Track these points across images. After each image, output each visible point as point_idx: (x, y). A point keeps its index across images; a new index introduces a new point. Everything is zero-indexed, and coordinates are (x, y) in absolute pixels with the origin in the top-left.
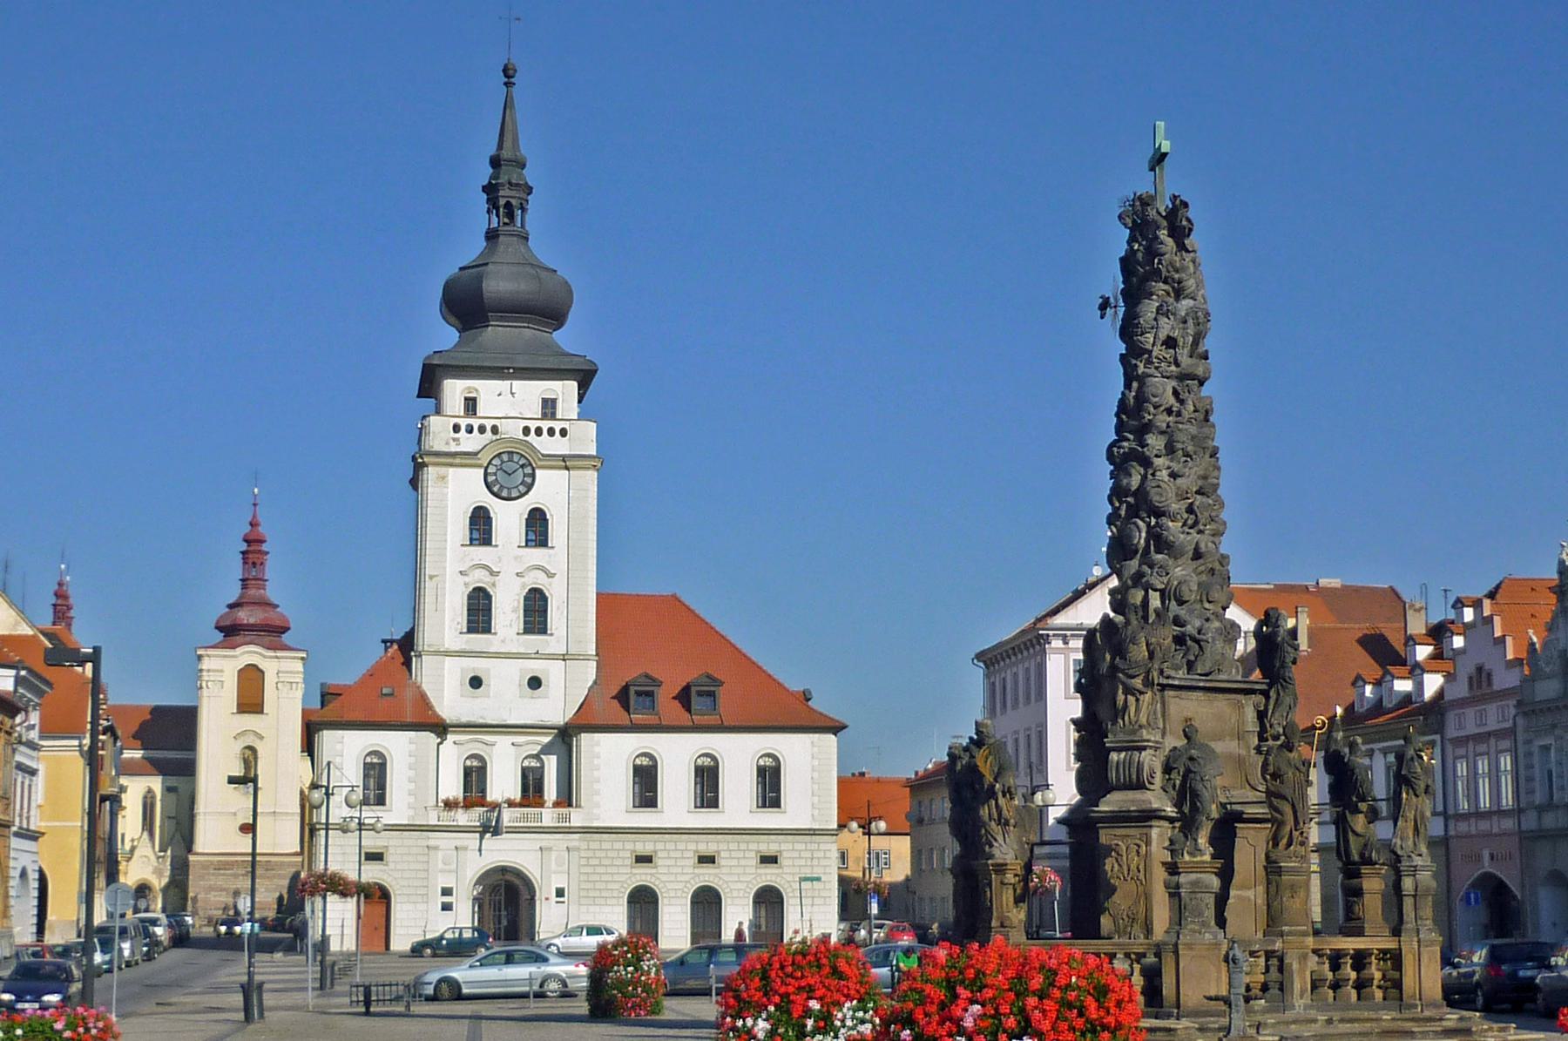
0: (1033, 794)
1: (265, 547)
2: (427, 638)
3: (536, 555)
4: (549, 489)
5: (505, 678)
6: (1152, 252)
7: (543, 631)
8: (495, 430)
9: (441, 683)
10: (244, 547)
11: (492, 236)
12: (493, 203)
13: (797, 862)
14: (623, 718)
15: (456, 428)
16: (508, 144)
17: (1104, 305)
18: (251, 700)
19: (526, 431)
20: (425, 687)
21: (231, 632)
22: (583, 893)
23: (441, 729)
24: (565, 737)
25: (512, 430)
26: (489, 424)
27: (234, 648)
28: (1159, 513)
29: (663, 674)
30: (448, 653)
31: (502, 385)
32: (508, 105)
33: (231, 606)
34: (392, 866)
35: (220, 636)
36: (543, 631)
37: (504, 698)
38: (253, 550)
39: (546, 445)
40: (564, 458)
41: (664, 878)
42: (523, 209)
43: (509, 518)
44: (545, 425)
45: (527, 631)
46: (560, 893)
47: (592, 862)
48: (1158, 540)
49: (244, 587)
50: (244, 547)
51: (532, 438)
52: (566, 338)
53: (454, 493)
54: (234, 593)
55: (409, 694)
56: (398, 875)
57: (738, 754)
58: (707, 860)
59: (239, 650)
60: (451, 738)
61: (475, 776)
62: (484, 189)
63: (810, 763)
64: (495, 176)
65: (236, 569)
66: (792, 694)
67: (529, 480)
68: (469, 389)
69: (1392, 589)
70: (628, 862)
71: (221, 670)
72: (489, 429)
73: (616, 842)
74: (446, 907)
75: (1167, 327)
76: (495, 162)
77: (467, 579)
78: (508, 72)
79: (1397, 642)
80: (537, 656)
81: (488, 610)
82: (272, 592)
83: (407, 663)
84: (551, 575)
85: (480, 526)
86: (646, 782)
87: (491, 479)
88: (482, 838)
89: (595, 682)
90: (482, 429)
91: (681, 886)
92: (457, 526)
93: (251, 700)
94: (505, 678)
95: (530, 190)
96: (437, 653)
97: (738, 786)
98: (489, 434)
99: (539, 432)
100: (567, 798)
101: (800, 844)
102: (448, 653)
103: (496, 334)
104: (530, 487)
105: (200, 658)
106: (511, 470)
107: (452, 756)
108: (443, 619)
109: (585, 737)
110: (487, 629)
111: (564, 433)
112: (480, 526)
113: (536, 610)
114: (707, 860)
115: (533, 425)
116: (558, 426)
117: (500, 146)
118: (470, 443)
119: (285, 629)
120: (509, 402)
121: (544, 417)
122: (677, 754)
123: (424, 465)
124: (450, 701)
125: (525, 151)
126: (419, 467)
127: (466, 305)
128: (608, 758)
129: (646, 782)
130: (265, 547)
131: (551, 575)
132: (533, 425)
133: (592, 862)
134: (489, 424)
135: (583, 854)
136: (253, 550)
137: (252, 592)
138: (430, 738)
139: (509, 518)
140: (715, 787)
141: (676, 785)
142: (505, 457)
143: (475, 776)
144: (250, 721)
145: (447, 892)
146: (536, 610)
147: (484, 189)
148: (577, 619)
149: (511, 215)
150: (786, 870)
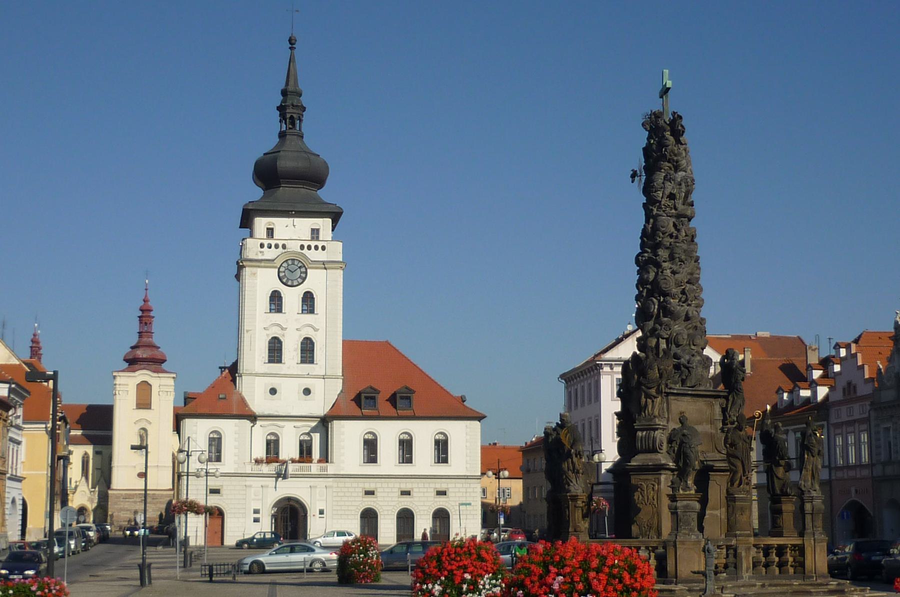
1: (152, 314)
2: (245, 366)
3: (308, 318)
4: (315, 281)
6: (662, 144)
7: (312, 362)
8: (284, 247)
9: (253, 390)
10: (140, 314)
11: (282, 135)
12: (283, 117)
14: (358, 412)
15: (262, 246)
16: (291, 82)
17: (634, 175)
18: (144, 402)
19: (302, 247)
20: (244, 394)
21: (133, 363)
22: (335, 512)
23: (253, 418)
24: (324, 423)
25: (294, 247)
26: (280, 243)
27: (134, 371)
28: (666, 294)
29: (382, 388)
30: (257, 375)
32: (291, 60)
33: (132, 348)
35: (126, 365)
36: (312, 362)
37: (290, 400)
38: (145, 316)
39: (313, 255)
40: (324, 263)
41: (381, 504)
42: (301, 120)
43: (292, 297)
44: (313, 244)
45: (302, 362)
46: (321, 512)
48: (665, 310)
49: (140, 337)
50: (140, 314)
51: (305, 251)
52: (326, 194)
53: (260, 283)
54: (134, 340)
55: (235, 398)
57: (424, 433)
58: (370, 493)
59: (137, 373)
60: (259, 423)
61: (273, 446)
62: (278, 108)
63: (465, 438)
64: (284, 101)
65: (135, 327)
66: (455, 398)
67: (304, 275)
69: (799, 337)
70: (361, 494)
71: (127, 385)
74: (256, 520)
75: (670, 187)
76: (284, 93)
77: (268, 332)
78: (292, 41)
79: (802, 368)
80: (308, 376)
81: (280, 350)
82: (156, 340)
83: (234, 381)
84: (316, 330)
85: (276, 301)
86: (371, 448)
87: (281, 275)
89: (342, 391)
90: (277, 246)
91: (391, 508)
92: (264, 302)
93: (144, 402)
94: (290, 390)
95: (304, 109)
96: (251, 374)
97: (424, 450)
98: (280, 249)
99: (309, 248)
100: (325, 457)
101: (459, 483)
102: (257, 375)
103: (285, 191)
104: (304, 279)
105: (115, 377)
106: (293, 270)
107: (260, 433)
108: (254, 355)
109: (336, 423)
110: (279, 361)
111: (323, 248)
112: (276, 301)
113: (307, 350)
114: (370, 493)
115: (306, 244)
116: (320, 244)
117: (287, 84)
118: (270, 254)
119: (164, 361)
120: (292, 231)
121: (313, 239)
122: (389, 432)
123: (243, 267)
124: (258, 402)
125: (301, 86)
126: (240, 268)
127: (268, 174)
128: (349, 435)
129: (371, 448)
130: (152, 314)
131: (316, 330)
132: (306, 244)
134: (280, 243)
136: (145, 316)
137: (145, 339)
138: (247, 423)
139: (292, 297)
140: (410, 451)
141: (388, 450)
143: (273, 446)
144: (143, 413)
145: (256, 511)
146: (307, 350)
147: (278, 108)
148: (330, 355)
149: (293, 124)
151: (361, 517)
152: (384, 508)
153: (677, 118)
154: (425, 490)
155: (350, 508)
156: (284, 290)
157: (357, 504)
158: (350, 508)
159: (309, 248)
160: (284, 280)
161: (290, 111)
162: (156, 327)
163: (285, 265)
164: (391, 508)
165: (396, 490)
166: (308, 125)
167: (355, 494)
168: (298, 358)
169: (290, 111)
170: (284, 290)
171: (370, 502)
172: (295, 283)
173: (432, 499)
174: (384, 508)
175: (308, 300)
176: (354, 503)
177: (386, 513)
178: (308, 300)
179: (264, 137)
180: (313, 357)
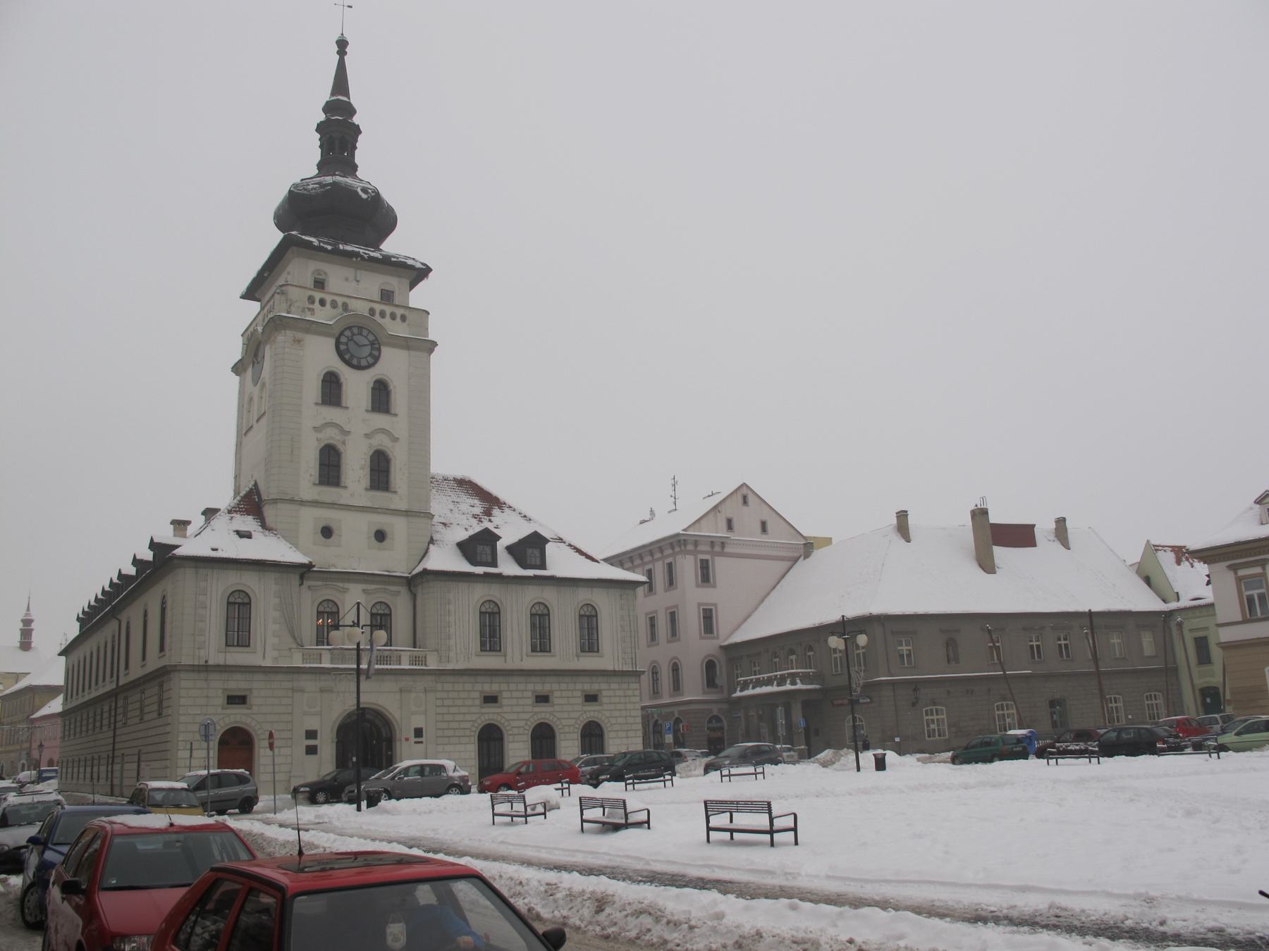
3: (380, 420)
5: (354, 529)
8: (345, 306)
13: (613, 700)
15: (311, 300)
19: (372, 311)
22: (440, 733)
25: (361, 308)
30: (302, 503)
31: (349, 272)
34: (255, 709)
41: (559, 715)
43: (357, 385)
46: (418, 732)
47: (446, 702)
52: (392, 246)
56: (608, 714)
58: (543, 699)
67: (376, 353)
68: (318, 272)
70: (478, 702)
72: (340, 304)
74: (311, 750)
77: (320, 436)
78: (342, 45)
80: (332, 505)
81: (387, 471)
85: (331, 390)
87: (342, 347)
90: (334, 305)
91: (572, 722)
92: (313, 389)
94: (354, 529)
99: (383, 314)
102: (302, 503)
104: (377, 359)
111: (403, 318)
112: (331, 390)
125: (355, 100)
131: (396, 440)
133: (446, 702)
135: (439, 695)
139: (357, 385)
142: (355, 331)
145: (311, 734)
147: (434, 344)
150: (506, 709)
151: (533, 738)
152: (613, 721)
154: (570, 694)
155: (463, 725)
157: (473, 717)
158: (463, 725)
159: (383, 314)
160: (347, 357)
161: (338, 133)
163: (348, 333)
164: (572, 722)
165: (529, 694)
166: (362, 155)
167: (469, 702)
168: (366, 482)
169: (338, 133)
171: (490, 714)
172: (364, 363)
173: (219, 710)
174: (613, 721)
175: (381, 397)
176: (468, 717)
177: (515, 731)
178: (381, 397)
180: (387, 482)
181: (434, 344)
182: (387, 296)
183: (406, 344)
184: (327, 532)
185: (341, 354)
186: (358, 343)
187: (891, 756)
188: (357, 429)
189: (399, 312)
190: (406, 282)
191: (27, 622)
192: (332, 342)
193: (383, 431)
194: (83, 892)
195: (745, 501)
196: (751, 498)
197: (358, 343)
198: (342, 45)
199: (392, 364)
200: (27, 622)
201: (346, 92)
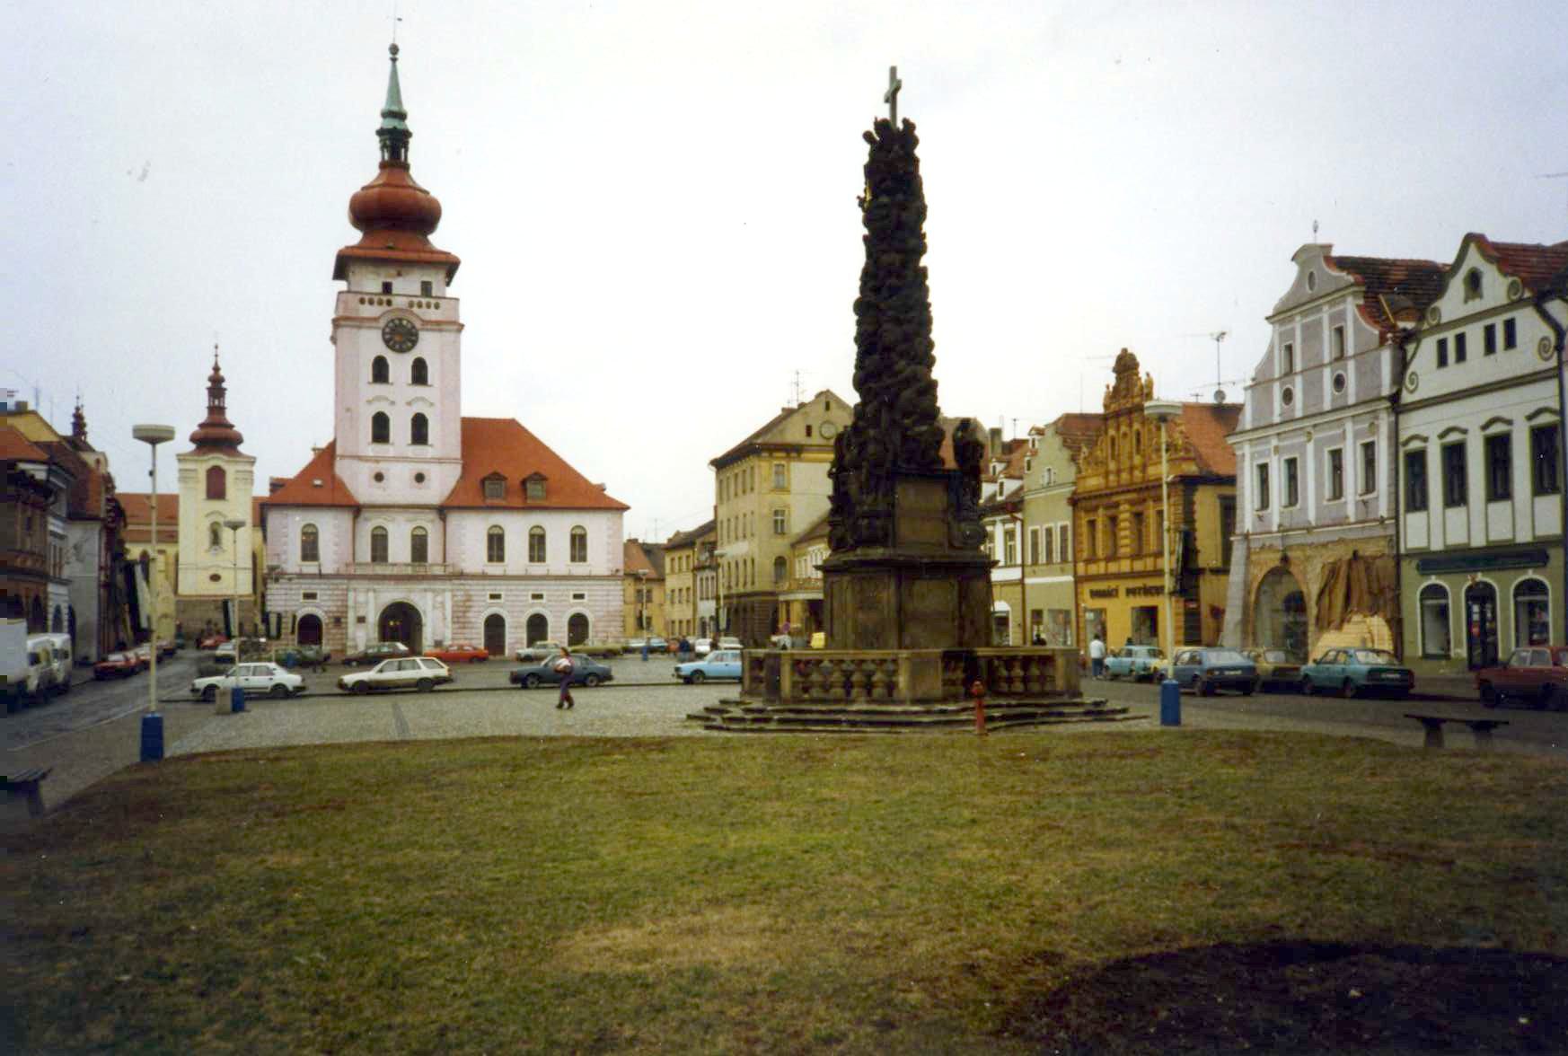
0: (1462, 789)
14: (479, 502)
19: (411, 305)
23: (357, 510)
24: (442, 511)
30: (359, 458)
35: (192, 447)
37: (399, 487)
40: (438, 323)
43: (400, 366)
44: (424, 301)
51: (415, 309)
52: (439, 239)
57: (558, 528)
61: (380, 543)
73: (521, 585)
78: (394, 50)
85: (380, 371)
86: (496, 545)
88: (613, 577)
92: (367, 372)
97: (558, 546)
101: (553, 585)
102: (359, 458)
104: (414, 343)
112: (380, 371)
122: (516, 529)
124: (364, 490)
125: (407, 106)
128: (470, 533)
129: (496, 545)
130: (871, 128)
139: (400, 366)
141: (516, 546)
147: (462, 326)
153: (909, 126)
156: (391, 357)
159: (420, 305)
161: (395, 140)
162: (230, 401)
169: (395, 140)
170: (391, 357)
175: (420, 373)
178: (420, 373)
179: (365, 168)
181: (462, 326)
182: (426, 288)
183: (438, 326)
184: (379, 477)
185: (387, 342)
186: (401, 336)
187: (574, 694)
188: (400, 400)
189: (433, 301)
190: (441, 276)
191: (892, 167)
192: (379, 333)
193: (422, 399)
194: (946, 478)
195: (828, 407)
196: (833, 405)
197: (401, 336)
198: (394, 50)
199: (428, 346)
200: (892, 167)
201: (399, 102)
